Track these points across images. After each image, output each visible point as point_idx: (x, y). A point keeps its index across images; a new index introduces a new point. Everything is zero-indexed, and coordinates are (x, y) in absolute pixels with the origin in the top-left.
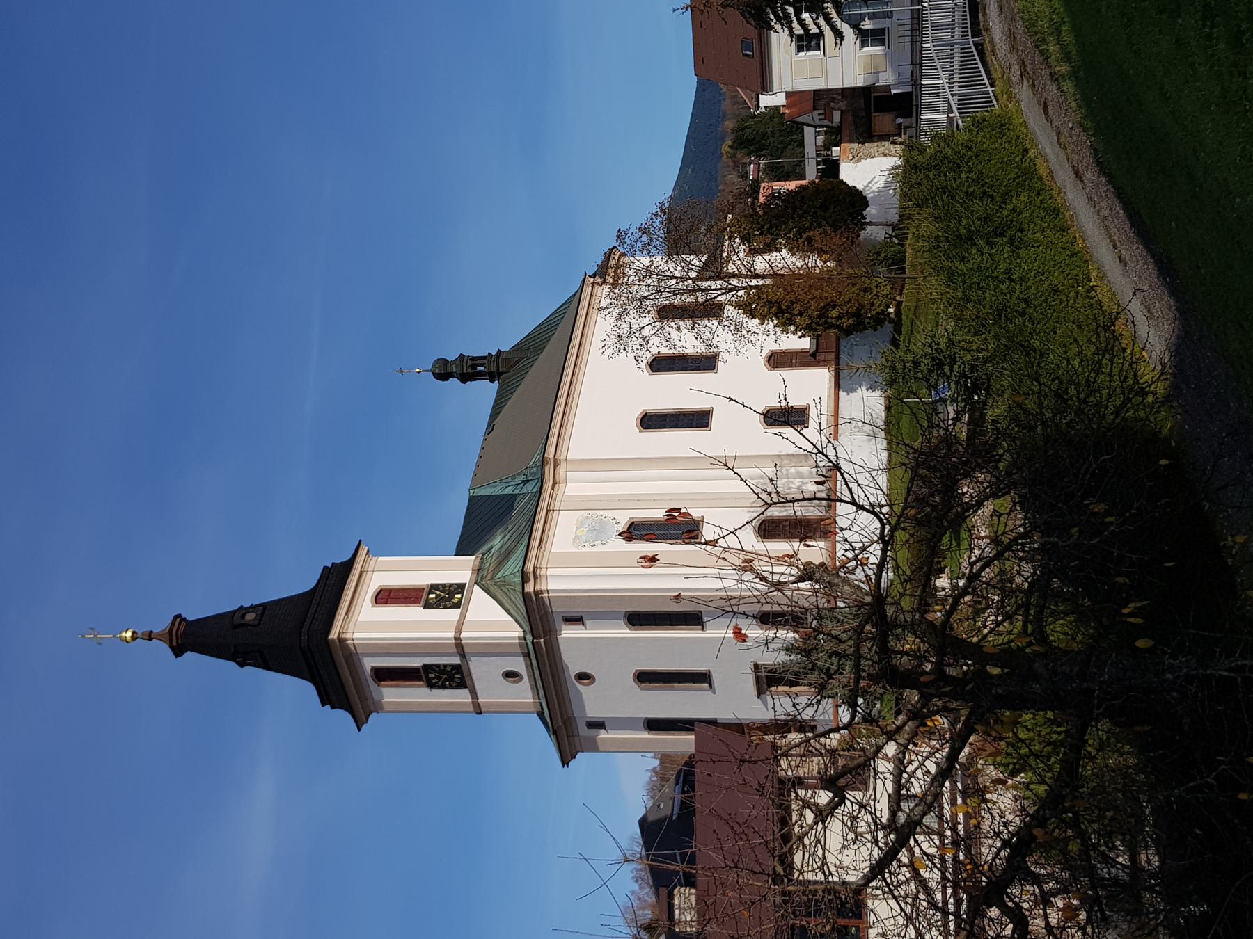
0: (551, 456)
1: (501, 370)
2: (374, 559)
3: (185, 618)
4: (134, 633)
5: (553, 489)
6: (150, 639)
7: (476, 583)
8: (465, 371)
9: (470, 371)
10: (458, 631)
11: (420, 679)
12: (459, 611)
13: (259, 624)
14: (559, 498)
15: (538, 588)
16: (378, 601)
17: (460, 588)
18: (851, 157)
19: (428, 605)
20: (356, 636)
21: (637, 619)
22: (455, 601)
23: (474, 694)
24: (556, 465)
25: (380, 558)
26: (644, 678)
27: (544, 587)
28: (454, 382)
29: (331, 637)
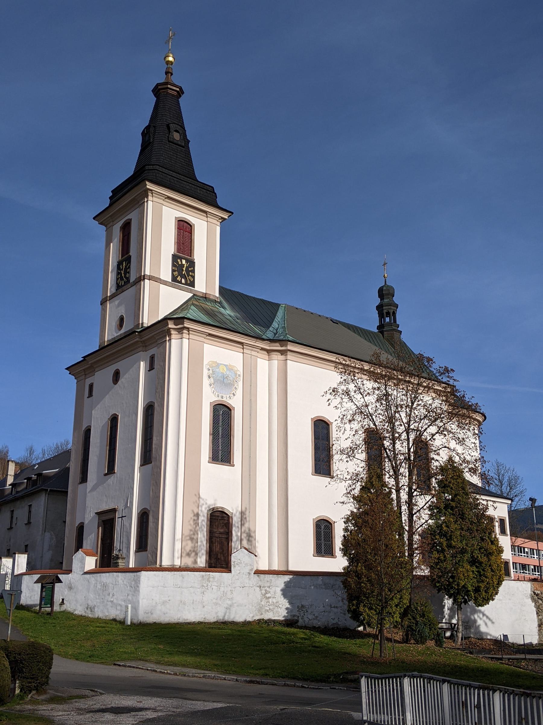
0: (289, 347)
1: (385, 333)
2: (219, 224)
3: (180, 96)
4: (171, 63)
5: (262, 349)
6: (167, 73)
7: (194, 294)
8: (384, 308)
9: (385, 311)
10: (151, 278)
11: (122, 256)
12: (170, 280)
13: (169, 141)
14: (254, 353)
15: (173, 332)
16: (182, 223)
17: (192, 284)
18: (537, 592)
19: (175, 258)
20: (150, 203)
21: (149, 410)
22: (179, 278)
23: (113, 296)
24: (283, 353)
25: (218, 229)
26: (114, 420)
27: (173, 336)
28: (378, 301)
29: (147, 183)
